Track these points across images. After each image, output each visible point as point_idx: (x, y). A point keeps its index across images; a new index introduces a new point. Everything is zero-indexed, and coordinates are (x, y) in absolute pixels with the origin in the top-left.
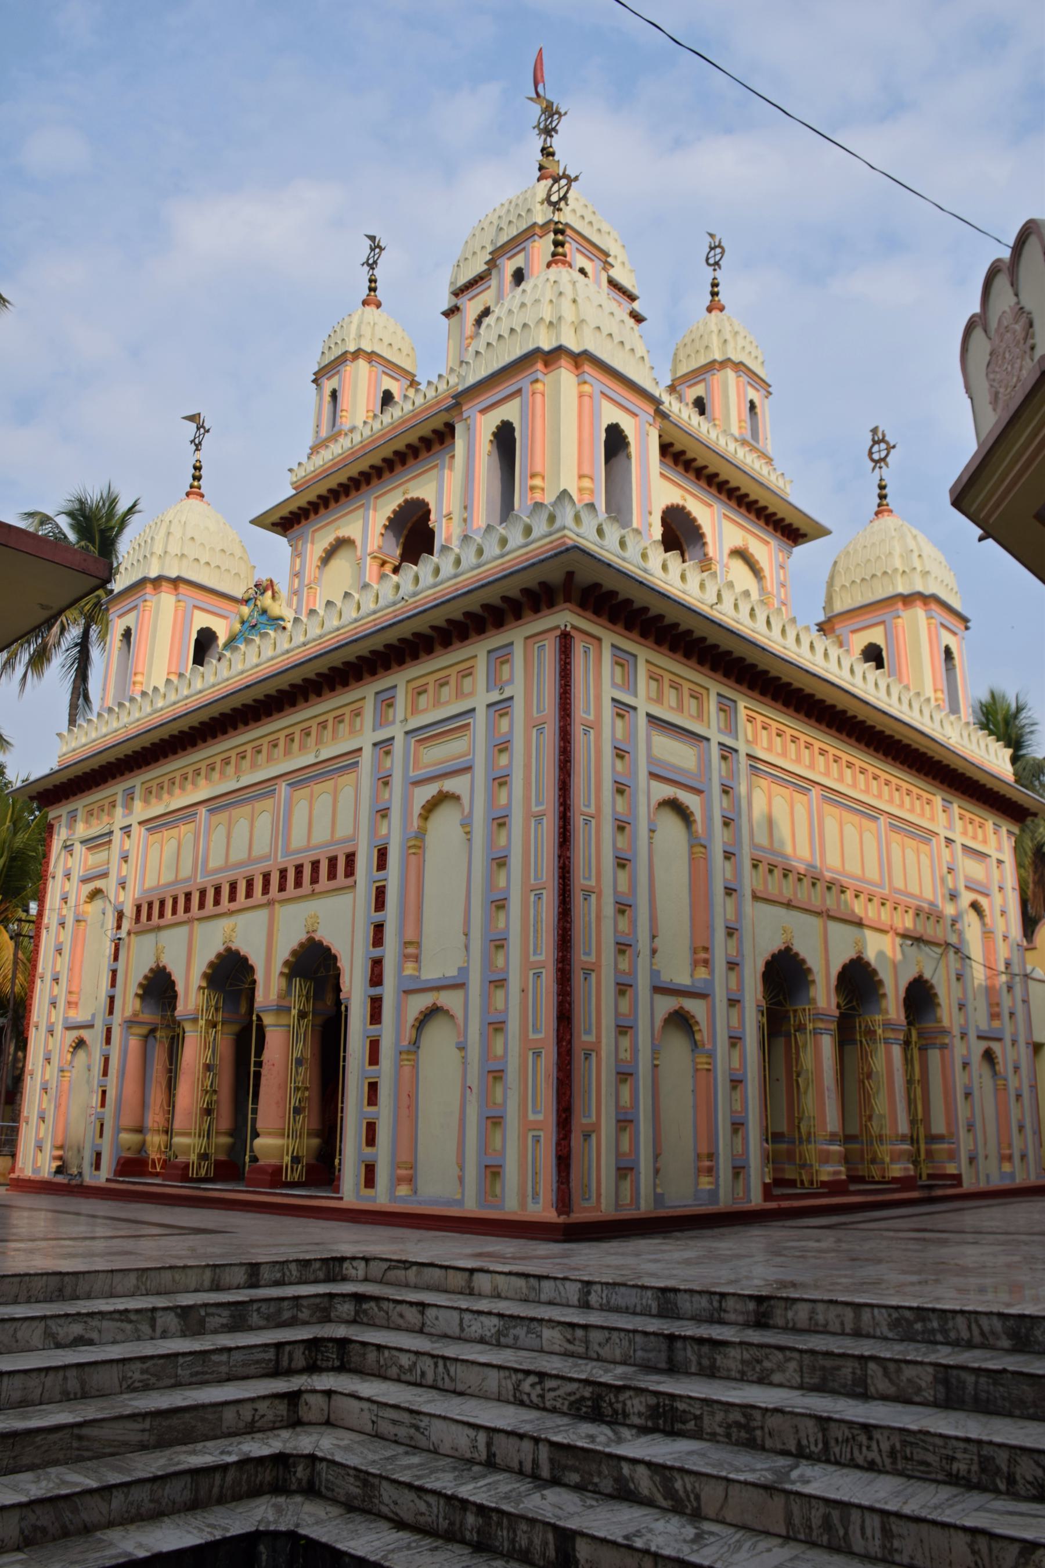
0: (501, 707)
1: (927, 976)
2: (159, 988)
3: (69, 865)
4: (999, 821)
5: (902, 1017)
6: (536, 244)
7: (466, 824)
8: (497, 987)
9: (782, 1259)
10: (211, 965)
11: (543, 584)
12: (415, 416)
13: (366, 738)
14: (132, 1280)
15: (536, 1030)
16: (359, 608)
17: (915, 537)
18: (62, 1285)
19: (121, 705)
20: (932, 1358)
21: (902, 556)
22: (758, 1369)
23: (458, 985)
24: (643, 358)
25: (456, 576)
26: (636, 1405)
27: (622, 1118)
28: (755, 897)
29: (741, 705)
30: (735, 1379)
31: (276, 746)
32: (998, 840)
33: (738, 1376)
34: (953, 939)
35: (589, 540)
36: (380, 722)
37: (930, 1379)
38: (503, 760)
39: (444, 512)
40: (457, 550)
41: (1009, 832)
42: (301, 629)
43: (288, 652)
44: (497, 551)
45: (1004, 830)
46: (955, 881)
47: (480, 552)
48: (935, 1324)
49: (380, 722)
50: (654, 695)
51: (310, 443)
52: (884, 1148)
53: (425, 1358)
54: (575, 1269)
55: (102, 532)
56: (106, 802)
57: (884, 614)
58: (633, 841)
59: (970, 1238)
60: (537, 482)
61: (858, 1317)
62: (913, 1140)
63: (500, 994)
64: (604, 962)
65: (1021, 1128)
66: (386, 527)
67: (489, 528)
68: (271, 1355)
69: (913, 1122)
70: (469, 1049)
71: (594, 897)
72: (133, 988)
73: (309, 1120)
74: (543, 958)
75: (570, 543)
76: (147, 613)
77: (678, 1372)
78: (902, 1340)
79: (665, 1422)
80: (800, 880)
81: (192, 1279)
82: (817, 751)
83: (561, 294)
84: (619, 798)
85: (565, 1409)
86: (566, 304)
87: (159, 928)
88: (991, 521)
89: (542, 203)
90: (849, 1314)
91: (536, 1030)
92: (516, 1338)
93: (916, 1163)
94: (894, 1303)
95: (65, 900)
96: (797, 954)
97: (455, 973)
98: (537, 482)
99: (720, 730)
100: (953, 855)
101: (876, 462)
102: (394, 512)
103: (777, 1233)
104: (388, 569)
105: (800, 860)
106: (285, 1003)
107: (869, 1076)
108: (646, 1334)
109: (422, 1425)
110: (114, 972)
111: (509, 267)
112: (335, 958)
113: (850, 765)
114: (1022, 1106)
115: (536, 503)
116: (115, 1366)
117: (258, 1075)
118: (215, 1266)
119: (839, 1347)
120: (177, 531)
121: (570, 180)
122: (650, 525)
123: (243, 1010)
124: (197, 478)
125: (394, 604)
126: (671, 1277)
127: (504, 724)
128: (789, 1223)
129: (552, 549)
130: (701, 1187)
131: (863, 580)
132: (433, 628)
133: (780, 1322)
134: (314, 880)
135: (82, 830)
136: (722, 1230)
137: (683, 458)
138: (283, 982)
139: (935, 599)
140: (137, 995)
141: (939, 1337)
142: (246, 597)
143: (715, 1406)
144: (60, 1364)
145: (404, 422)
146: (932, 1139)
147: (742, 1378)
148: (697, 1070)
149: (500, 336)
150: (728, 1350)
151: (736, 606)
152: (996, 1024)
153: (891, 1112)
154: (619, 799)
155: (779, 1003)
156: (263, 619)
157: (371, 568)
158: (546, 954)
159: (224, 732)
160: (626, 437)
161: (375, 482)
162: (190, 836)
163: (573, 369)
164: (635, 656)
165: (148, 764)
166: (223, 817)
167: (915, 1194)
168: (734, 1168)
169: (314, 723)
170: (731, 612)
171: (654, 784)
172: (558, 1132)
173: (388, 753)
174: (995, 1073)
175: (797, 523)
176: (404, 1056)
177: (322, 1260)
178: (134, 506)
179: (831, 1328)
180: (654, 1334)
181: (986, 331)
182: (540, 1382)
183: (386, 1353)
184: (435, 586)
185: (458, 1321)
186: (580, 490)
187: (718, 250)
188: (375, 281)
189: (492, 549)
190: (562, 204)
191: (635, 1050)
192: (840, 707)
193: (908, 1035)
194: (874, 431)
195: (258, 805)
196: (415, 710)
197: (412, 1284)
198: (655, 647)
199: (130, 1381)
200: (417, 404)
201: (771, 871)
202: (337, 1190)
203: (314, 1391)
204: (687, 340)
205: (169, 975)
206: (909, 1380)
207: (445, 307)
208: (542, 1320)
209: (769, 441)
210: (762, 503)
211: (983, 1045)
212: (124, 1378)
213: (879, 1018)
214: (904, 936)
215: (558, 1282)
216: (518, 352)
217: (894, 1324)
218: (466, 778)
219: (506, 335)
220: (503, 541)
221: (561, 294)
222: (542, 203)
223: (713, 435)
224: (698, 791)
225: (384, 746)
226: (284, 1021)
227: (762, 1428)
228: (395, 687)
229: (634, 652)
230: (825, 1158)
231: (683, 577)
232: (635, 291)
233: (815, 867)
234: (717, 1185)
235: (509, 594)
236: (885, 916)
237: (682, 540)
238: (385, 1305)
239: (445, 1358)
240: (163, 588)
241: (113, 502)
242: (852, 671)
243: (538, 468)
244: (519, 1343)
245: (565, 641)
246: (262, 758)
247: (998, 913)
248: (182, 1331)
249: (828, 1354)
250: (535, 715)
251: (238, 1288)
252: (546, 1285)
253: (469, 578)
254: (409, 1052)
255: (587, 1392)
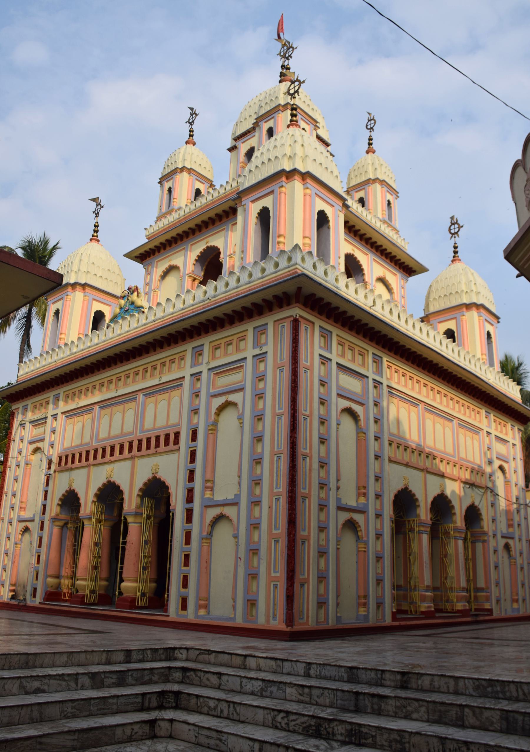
0: (261, 357)
1: (476, 504)
2: (70, 501)
3: (23, 434)
4: (514, 424)
5: (464, 525)
6: (280, 115)
7: (241, 418)
8: (255, 505)
9: (409, 652)
10: (99, 489)
11: (285, 293)
12: (213, 203)
13: (187, 371)
14: (64, 658)
15: (276, 528)
16: (184, 303)
17: (473, 274)
18: (28, 660)
19: (53, 350)
20: (499, 706)
21: (466, 284)
22: (404, 711)
23: (235, 503)
24: (337, 176)
25: (237, 287)
26: (340, 729)
27: (320, 576)
28: (390, 461)
29: (385, 359)
30: (392, 716)
31: (137, 374)
32: (513, 435)
33: (393, 714)
34: (490, 485)
35: (309, 270)
36: (195, 363)
37: (498, 717)
38: (261, 385)
39: (228, 254)
40: (238, 274)
41: (519, 429)
42: (152, 313)
43: (145, 324)
44: (260, 275)
45: (516, 428)
46: (491, 454)
47: (251, 275)
48: (499, 688)
49: (195, 363)
50: (340, 353)
51: (156, 215)
52: (454, 594)
53: (223, 702)
54: (301, 656)
55: (40, 258)
56: (44, 401)
57: (456, 314)
58: (328, 429)
59: (496, 642)
60: (281, 239)
61: (456, 684)
62: (468, 590)
63: (257, 509)
64: (313, 493)
65: (523, 585)
66: (196, 260)
67: (256, 263)
68: (139, 699)
69: (468, 581)
70: (240, 537)
71: (308, 459)
72: (56, 501)
73: (150, 574)
74: (281, 490)
75: (300, 272)
76: (68, 302)
77: (361, 712)
78: (480, 697)
79: (355, 739)
80: (413, 452)
81: (96, 658)
82: (422, 384)
83: (295, 141)
84: (321, 407)
85: (300, 731)
86: (298, 146)
87: (71, 469)
88: (525, 267)
89: (285, 94)
90: (452, 682)
91: (276, 528)
92: (271, 692)
93: (469, 602)
94: (476, 677)
95: (20, 453)
96: (411, 491)
97: (233, 497)
98: (281, 239)
99: (373, 373)
100: (490, 441)
101: (453, 234)
102: (201, 253)
103: (401, 638)
104: (197, 282)
105: (413, 442)
106: (139, 511)
107: (446, 556)
108: (343, 691)
109: (224, 738)
110: (46, 492)
111: (265, 126)
112: (167, 488)
113: (439, 392)
114: (524, 573)
115: (281, 251)
116: (58, 704)
117: (124, 549)
118: (108, 651)
119: (448, 700)
120: (85, 260)
121: (300, 83)
122: (339, 264)
123: (115, 514)
124: (96, 231)
125: (204, 301)
126: (353, 661)
127: (262, 366)
128: (405, 633)
129: (290, 275)
130: (360, 613)
131: (445, 295)
132: (225, 314)
133: (414, 686)
134: (157, 446)
135: (30, 416)
136: (371, 636)
137: (354, 229)
138: (139, 500)
139: (483, 306)
140: (58, 504)
141: (501, 695)
142: (123, 295)
143: (383, 731)
144: (29, 703)
145: (207, 206)
146: (478, 590)
147: (396, 716)
148: (359, 551)
149: (263, 163)
150: (388, 700)
151: (383, 307)
152: (511, 530)
153: (457, 575)
154: (322, 407)
155: (401, 517)
156: (132, 307)
157: (188, 282)
158: (282, 488)
159: (110, 366)
160: (328, 217)
161: (191, 236)
162: (89, 421)
163: (301, 180)
164: (331, 332)
165: (67, 382)
166: (108, 411)
167: (469, 619)
168: (377, 603)
169: (158, 363)
170: (380, 311)
171: (340, 400)
172: (287, 583)
173: (198, 380)
174: (510, 556)
175: (411, 265)
176: (204, 541)
177: (164, 649)
178: (57, 244)
179: (442, 689)
180: (348, 691)
181: (524, 169)
182: (287, 717)
183: (201, 700)
184: (226, 292)
185: (239, 683)
186: (304, 244)
187: (373, 122)
188: (193, 131)
189: (257, 274)
190: (296, 94)
191: (327, 540)
192: (435, 362)
193: (467, 533)
194: (452, 218)
195: (127, 405)
196: (214, 358)
197: (212, 663)
198: (342, 328)
199: (65, 713)
200: (214, 196)
201: (398, 447)
202: (166, 611)
203: (163, 720)
204: (356, 168)
205: (76, 494)
206: (487, 718)
207: (229, 146)
208: (286, 683)
209: (397, 222)
210: (393, 254)
211: (504, 541)
212: (63, 711)
213: (451, 525)
214: (465, 483)
215: (293, 663)
216: (272, 172)
217: (477, 688)
218: (241, 394)
219: (266, 162)
220: (263, 270)
221: (295, 141)
222: (285, 94)
223: (369, 218)
224: (362, 404)
225: (197, 376)
226: (139, 520)
227: (409, 743)
228: (203, 345)
229: (331, 330)
230: (423, 599)
231: (356, 292)
232: (329, 141)
233: (420, 446)
234: (368, 612)
235: (266, 298)
236: (456, 472)
237: (352, 272)
238: (199, 674)
239: (234, 703)
240: (77, 289)
241: (46, 243)
242: (441, 343)
243: (282, 232)
244: (273, 695)
245: (296, 324)
246: (129, 381)
247: (513, 472)
248: (92, 686)
249: (443, 703)
250: (279, 361)
251: (120, 663)
252: (286, 664)
253: (244, 289)
254: (207, 539)
255: (313, 722)
